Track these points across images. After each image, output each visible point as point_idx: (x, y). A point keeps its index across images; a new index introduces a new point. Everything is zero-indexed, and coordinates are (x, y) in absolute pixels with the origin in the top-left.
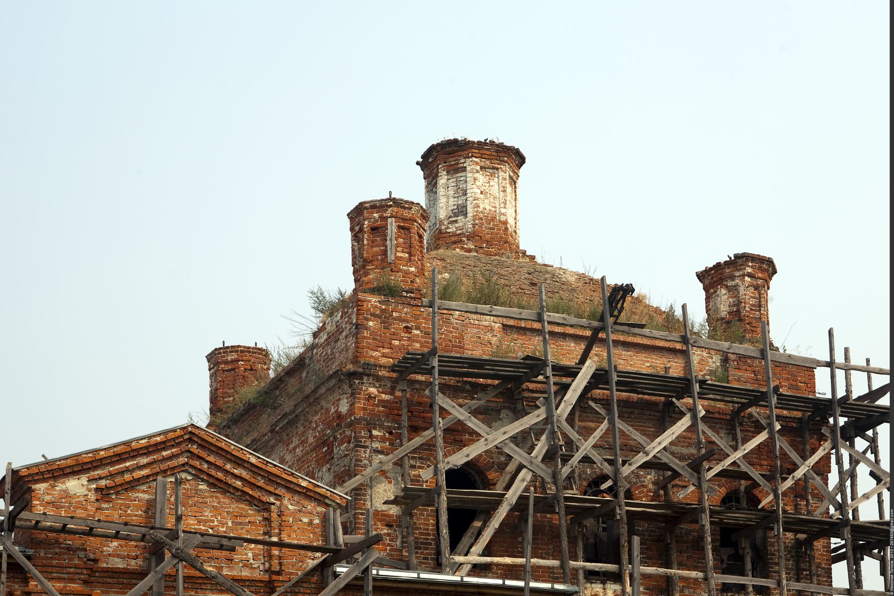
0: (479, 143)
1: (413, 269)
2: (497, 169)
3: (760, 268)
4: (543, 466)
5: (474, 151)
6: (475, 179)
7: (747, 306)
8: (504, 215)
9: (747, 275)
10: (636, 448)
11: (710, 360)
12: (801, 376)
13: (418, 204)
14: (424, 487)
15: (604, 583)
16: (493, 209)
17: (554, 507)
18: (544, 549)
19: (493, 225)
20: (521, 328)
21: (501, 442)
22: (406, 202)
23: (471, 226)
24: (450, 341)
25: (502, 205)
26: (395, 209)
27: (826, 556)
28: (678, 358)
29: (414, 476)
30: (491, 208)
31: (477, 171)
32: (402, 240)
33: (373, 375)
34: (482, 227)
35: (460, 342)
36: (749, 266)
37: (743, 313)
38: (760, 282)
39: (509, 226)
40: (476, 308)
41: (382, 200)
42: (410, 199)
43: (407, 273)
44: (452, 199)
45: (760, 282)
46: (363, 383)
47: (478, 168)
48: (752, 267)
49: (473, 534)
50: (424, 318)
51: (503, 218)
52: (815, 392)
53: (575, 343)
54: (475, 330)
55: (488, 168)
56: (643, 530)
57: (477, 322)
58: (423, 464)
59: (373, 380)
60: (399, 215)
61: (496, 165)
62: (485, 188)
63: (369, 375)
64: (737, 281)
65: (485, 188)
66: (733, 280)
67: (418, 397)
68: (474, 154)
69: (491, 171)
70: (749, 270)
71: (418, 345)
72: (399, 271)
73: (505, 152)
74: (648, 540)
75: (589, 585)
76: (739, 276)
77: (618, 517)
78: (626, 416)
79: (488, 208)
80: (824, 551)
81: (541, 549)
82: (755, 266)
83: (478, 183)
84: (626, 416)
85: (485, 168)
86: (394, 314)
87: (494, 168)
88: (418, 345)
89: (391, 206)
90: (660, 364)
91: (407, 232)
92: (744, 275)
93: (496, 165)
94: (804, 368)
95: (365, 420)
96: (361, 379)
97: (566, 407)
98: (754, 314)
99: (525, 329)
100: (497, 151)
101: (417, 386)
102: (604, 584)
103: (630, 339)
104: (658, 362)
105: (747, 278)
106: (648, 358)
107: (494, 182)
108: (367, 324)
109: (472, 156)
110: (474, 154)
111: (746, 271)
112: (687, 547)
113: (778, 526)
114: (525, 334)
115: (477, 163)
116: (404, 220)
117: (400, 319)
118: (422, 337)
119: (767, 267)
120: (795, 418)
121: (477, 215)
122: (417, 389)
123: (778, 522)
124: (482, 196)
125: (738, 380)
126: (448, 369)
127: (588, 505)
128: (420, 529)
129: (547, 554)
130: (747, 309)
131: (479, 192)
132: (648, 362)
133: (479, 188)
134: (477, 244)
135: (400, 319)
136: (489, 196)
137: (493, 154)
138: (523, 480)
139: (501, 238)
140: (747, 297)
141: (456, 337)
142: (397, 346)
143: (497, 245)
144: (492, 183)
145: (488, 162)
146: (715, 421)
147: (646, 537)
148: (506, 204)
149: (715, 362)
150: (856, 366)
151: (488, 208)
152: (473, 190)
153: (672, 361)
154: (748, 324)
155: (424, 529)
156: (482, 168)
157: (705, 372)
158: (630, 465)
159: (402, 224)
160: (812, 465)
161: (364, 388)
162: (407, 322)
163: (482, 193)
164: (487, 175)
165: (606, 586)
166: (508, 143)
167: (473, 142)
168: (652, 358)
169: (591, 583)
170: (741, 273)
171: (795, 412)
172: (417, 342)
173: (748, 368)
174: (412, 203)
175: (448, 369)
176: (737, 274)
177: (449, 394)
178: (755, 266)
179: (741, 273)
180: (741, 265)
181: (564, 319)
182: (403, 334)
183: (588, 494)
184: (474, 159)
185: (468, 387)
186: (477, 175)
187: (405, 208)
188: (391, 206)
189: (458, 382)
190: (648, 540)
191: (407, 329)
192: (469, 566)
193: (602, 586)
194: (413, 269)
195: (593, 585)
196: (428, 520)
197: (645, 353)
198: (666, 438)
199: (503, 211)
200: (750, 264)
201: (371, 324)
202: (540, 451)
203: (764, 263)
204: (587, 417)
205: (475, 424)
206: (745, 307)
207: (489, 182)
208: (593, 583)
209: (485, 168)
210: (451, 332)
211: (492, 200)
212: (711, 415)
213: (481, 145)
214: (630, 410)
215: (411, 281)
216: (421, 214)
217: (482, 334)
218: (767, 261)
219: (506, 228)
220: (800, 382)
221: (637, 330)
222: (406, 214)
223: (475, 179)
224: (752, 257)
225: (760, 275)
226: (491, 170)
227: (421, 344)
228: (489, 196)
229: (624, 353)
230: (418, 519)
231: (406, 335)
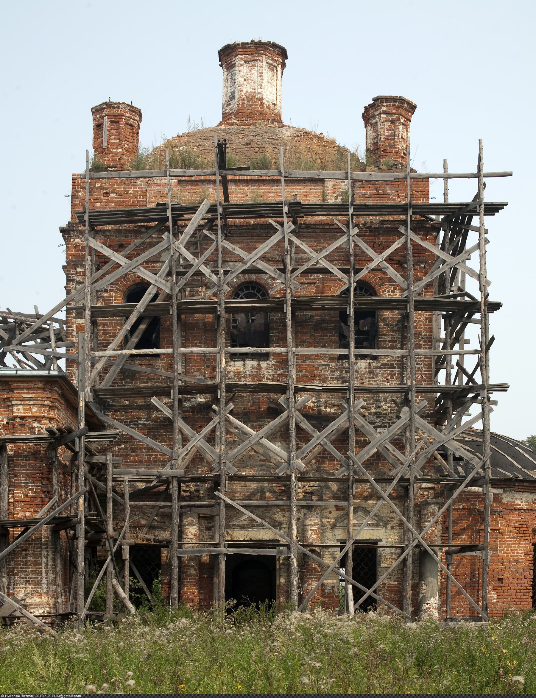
0: (243, 44)
1: (120, 150)
2: (257, 60)
3: (394, 106)
4: (164, 282)
5: (239, 50)
6: (240, 71)
7: (382, 137)
8: (260, 93)
9: (382, 113)
10: (272, 258)
11: (343, 184)
12: (416, 187)
13: (123, 103)
14: (114, 304)
15: (244, 360)
16: (253, 91)
17: (169, 310)
18: (198, 340)
19: (252, 102)
20: (193, 181)
21: (134, 268)
22: (115, 103)
23: (236, 106)
24: (136, 198)
25: (259, 87)
26: (108, 110)
27: (428, 325)
28: (318, 186)
29: (107, 297)
30: (252, 90)
31: (242, 65)
32: (114, 131)
33: (77, 230)
34: (243, 105)
35: (143, 198)
36: (384, 106)
37: (380, 143)
38: (395, 117)
39: (264, 101)
40: (119, 174)
41: (100, 105)
42: (117, 101)
43: (116, 153)
44: (229, 89)
45: (395, 117)
46: (71, 237)
47: (243, 62)
48: (387, 106)
49: (139, 334)
50: (118, 185)
51: (259, 96)
52: (429, 198)
53: (236, 186)
54: (158, 187)
55: (250, 61)
56: (276, 319)
57: (159, 181)
58: (112, 287)
59: (77, 233)
60: (110, 113)
61: (256, 58)
62: (247, 76)
63: (73, 231)
64: (377, 119)
65: (247, 76)
66: (375, 119)
67: (110, 241)
68: (240, 53)
69: (252, 63)
70: (384, 109)
71: (113, 204)
72: (111, 153)
73: (262, 47)
74: (280, 326)
75: (232, 363)
76: (377, 115)
77: (219, 313)
78: (264, 235)
79: (249, 90)
80: (426, 322)
81: (196, 340)
82: (390, 105)
83: (242, 73)
84: (264, 235)
85: (248, 62)
86: (97, 185)
87: (254, 60)
88: (113, 204)
89: (105, 108)
90: (303, 192)
91: (117, 124)
92: (380, 114)
93: (256, 58)
94: (420, 180)
95: (73, 261)
96: (70, 234)
97: (185, 236)
98: (390, 143)
99: (195, 181)
100: (256, 47)
101: (108, 234)
102: (244, 361)
103: (237, 178)
104: (301, 191)
105: (382, 116)
106: (293, 189)
107: (255, 72)
108: (78, 195)
109: (239, 54)
110: (240, 53)
111: (381, 110)
112: (310, 328)
113: (350, 307)
114: (197, 184)
115: (242, 59)
116: (115, 116)
117: (101, 188)
118: (116, 198)
119: (399, 105)
120: (401, 221)
121: (240, 97)
122: (108, 236)
123: (350, 304)
124: (245, 83)
125: (363, 196)
126: (116, 219)
127: (207, 306)
128: (110, 333)
129: (200, 343)
130: (382, 139)
131: (243, 80)
132: (293, 192)
133: (242, 77)
134: (239, 119)
135: (101, 188)
136: (250, 81)
137: (253, 50)
138: (150, 294)
139: (258, 111)
140: (383, 130)
141: (140, 195)
142: (99, 207)
143: (254, 117)
144: (253, 72)
145: (250, 57)
146: (336, 231)
147: (279, 324)
148: (262, 85)
149: (346, 185)
150: (433, 174)
151: (249, 90)
152: (240, 79)
153: (313, 189)
154: (383, 151)
155: (113, 333)
156: (245, 62)
157: (338, 194)
158: (232, 273)
159: (113, 119)
160: (385, 257)
161: (72, 240)
162: (106, 189)
163: (245, 80)
164: (249, 66)
165: (246, 362)
166: (265, 40)
167: (239, 44)
168: (297, 189)
169: (234, 361)
170: (378, 112)
171: (401, 216)
172: (112, 202)
173: (372, 186)
174: (119, 103)
175: (116, 219)
176: (376, 113)
177: (131, 236)
178: (390, 105)
179: (378, 112)
180: (378, 106)
181: (185, 172)
182: (103, 198)
183: (240, 297)
184: (239, 56)
185: (143, 229)
186: (241, 68)
187: (115, 108)
188: (105, 108)
189: (135, 227)
190: (280, 326)
191: (107, 194)
192: (106, 358)
193: (243, 362)
194: (120, 150)
195: (236, 363)
196: (116, 327)
197: (291, 186)
198: (261, 250)
199: (260, 91)
200: (385, 104)
201: (80, 194)
202: (164, 271)
203: (396, 102)
204: (234, 240)
205: (117, 258)
206: (380, 138)
207: (251, 71)
208: (236, 361)
209: (248, 62)
210: (137, 191)
211: (252, 84)
212: (331, 227)
213: (244, 45)
214: (266, 231)
215: (119, 159)
216: (129, 109)
217: (162, 189)
218: (399, 99)
219: (262, 104)
220: (416, 192)
221: (243, 172)
222: (116, 111)
223: (240, 71)
224: (385, 99)
225: (394, 111)
226: (251, 62)
227: (115, 202)
228: (250, 81)
229: (274, 188)
230: (108, 327)
231: (105, 198)
